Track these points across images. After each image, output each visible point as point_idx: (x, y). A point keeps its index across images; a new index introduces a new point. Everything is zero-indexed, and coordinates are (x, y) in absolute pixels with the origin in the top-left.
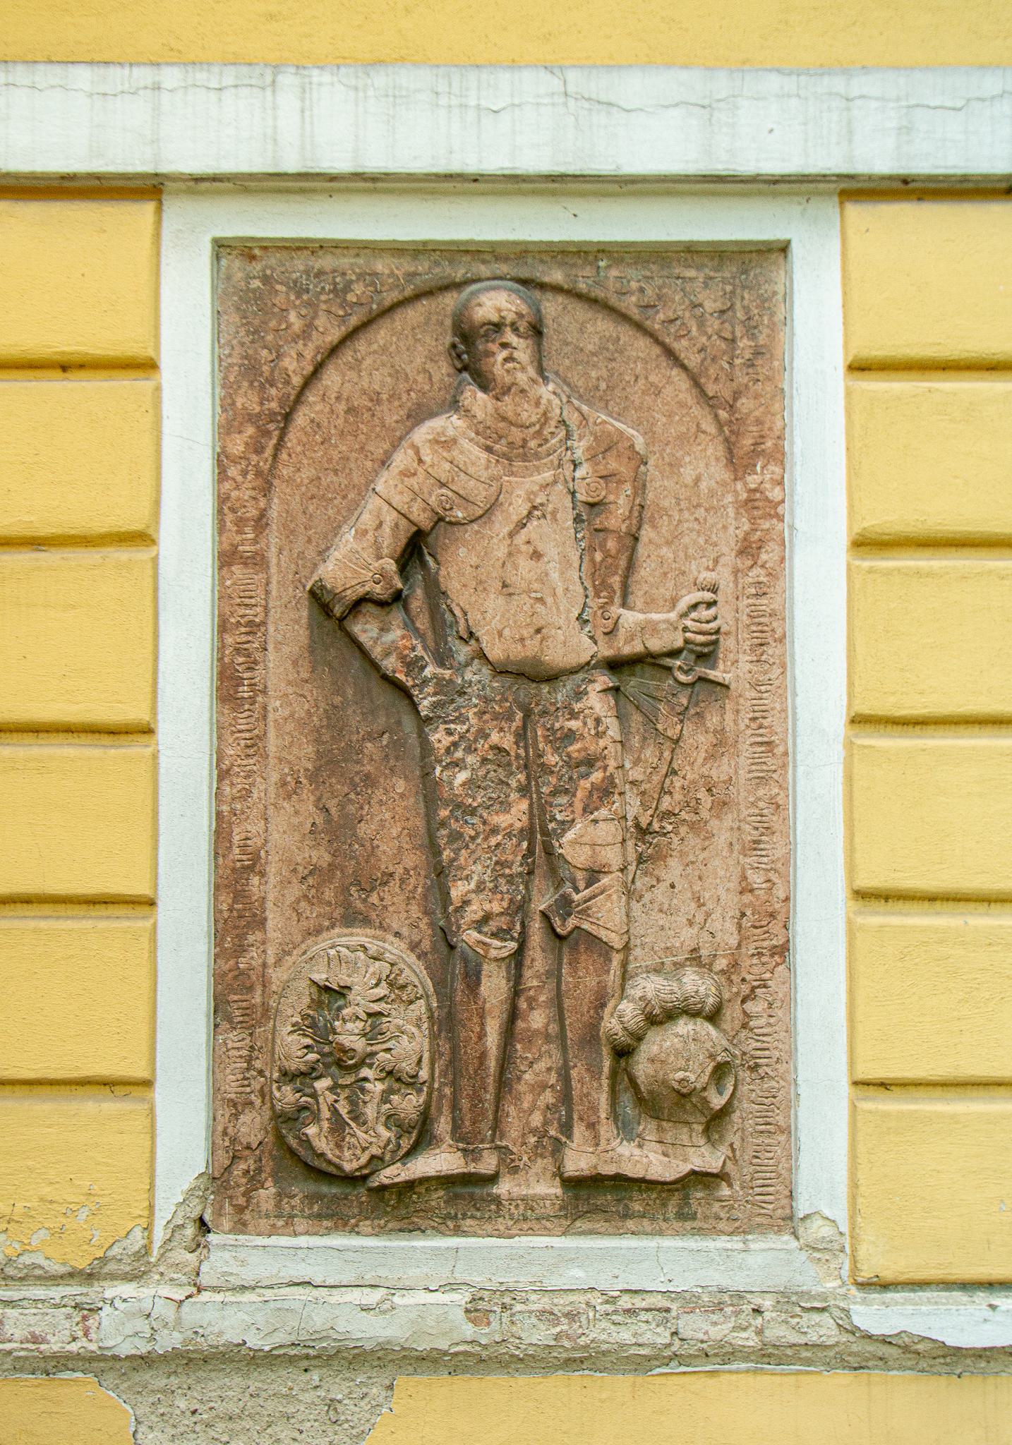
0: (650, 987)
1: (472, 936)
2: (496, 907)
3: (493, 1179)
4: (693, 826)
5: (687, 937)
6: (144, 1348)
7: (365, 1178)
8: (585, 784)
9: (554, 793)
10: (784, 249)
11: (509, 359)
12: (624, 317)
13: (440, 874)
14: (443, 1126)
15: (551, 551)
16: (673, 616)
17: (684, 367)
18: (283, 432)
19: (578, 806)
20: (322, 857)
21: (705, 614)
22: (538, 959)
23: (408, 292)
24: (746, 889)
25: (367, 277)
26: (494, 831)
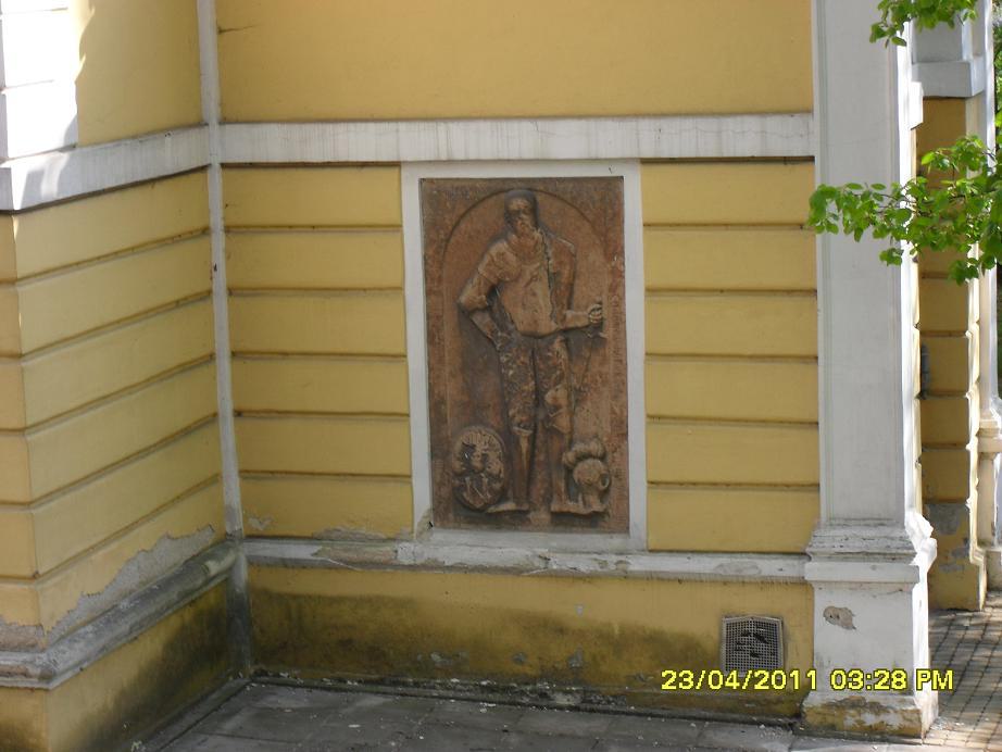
0: (579, 447)
1: (516, 428)
2: (524, 418)
3: (527, 512)
4: (595, 390)
5: (593, 429)
6: (412, 562)
7: (483, 511)
8: (554, 376)
9: (544, 378)
10: (622, 177)
11: (523, 223)
12: (566, 201)
13: (506, 406)
14: (510, 493)
15: (539, 292)
16: (585, 313)
17: (588, 221)
18: (446, 246)
19: (552, 384)
20: (466, 399)
21: (597, 313)
22: (540, 435)
23: (488, 194)
24: (613, 412)
25: (528, 433)
26: (523, 391)
